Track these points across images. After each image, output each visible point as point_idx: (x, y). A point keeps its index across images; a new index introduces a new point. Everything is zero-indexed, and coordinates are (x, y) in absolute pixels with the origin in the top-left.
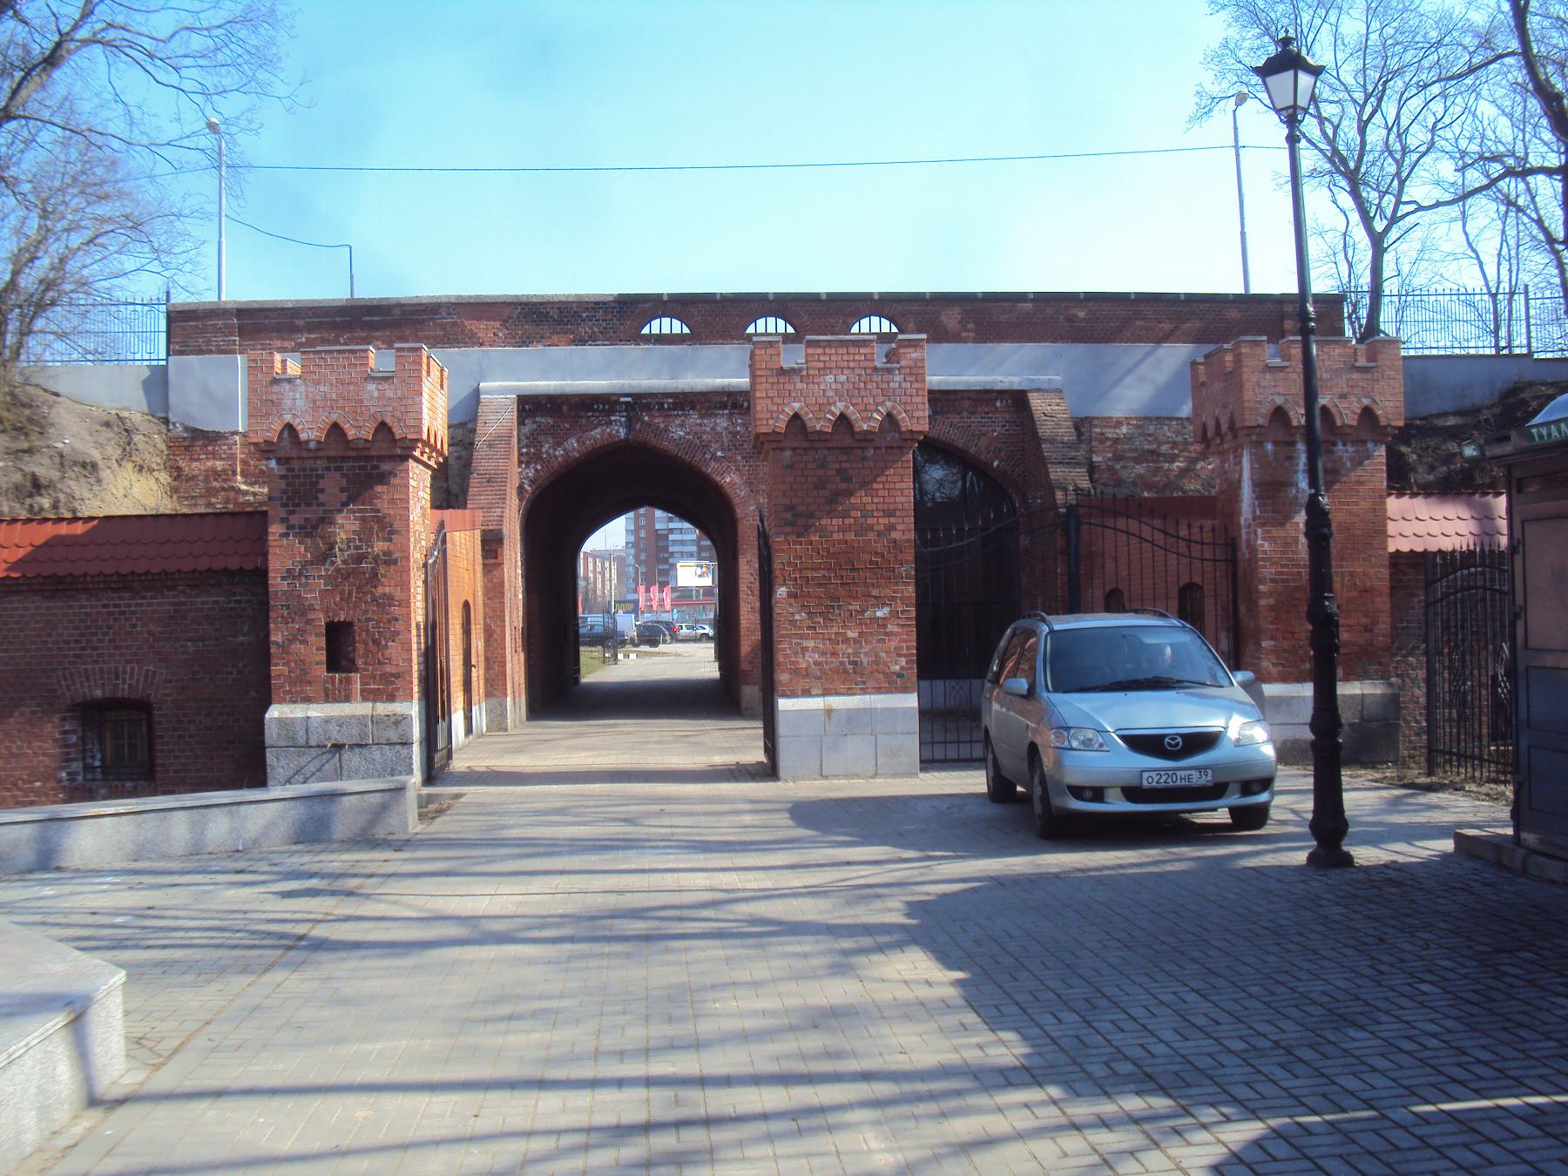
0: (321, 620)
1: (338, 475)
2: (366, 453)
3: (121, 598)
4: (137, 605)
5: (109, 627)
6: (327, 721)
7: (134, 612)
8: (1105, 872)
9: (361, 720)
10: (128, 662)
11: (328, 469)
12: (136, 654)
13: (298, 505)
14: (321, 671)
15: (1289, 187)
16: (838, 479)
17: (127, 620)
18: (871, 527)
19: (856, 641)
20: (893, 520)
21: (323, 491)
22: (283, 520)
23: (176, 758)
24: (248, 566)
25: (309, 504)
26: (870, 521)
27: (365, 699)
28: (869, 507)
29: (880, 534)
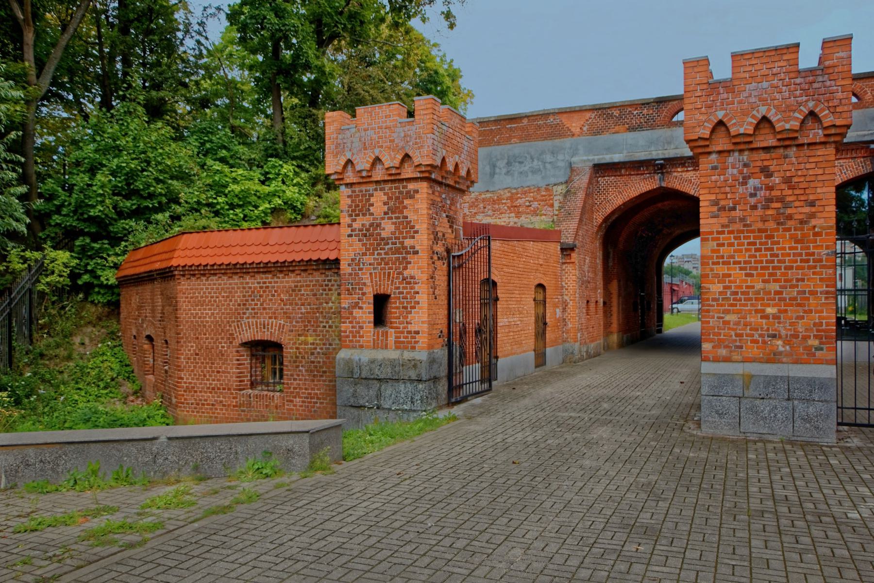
0: (370, 292)
1: (382, 193)
2: (398, 177)
3: (267, 278)
4: (275, 282)
5: (261, 296)
6: (372, 362)
7: (273, 287)
8: (614, 218)
9: (393, 363)
10: (270, 318)
11: (376, 190)
12: (275, 313)
13: (358, 215)
14: (369, 327)
15: (290, 430)
16: (772, 168)
17: (270, 291)
18: (790, 217)
19: (775, 317)
20: (813, 209)
21: (372, 205)
22: (350, 226)
23: (295, 379)
24: (332, 257)
25: (364, 215)
26: (789, 211)
27: (397, 348)
28: (789, 199)
29: (802, 222)
